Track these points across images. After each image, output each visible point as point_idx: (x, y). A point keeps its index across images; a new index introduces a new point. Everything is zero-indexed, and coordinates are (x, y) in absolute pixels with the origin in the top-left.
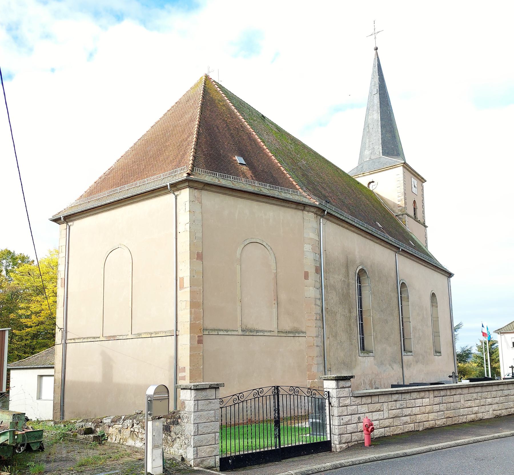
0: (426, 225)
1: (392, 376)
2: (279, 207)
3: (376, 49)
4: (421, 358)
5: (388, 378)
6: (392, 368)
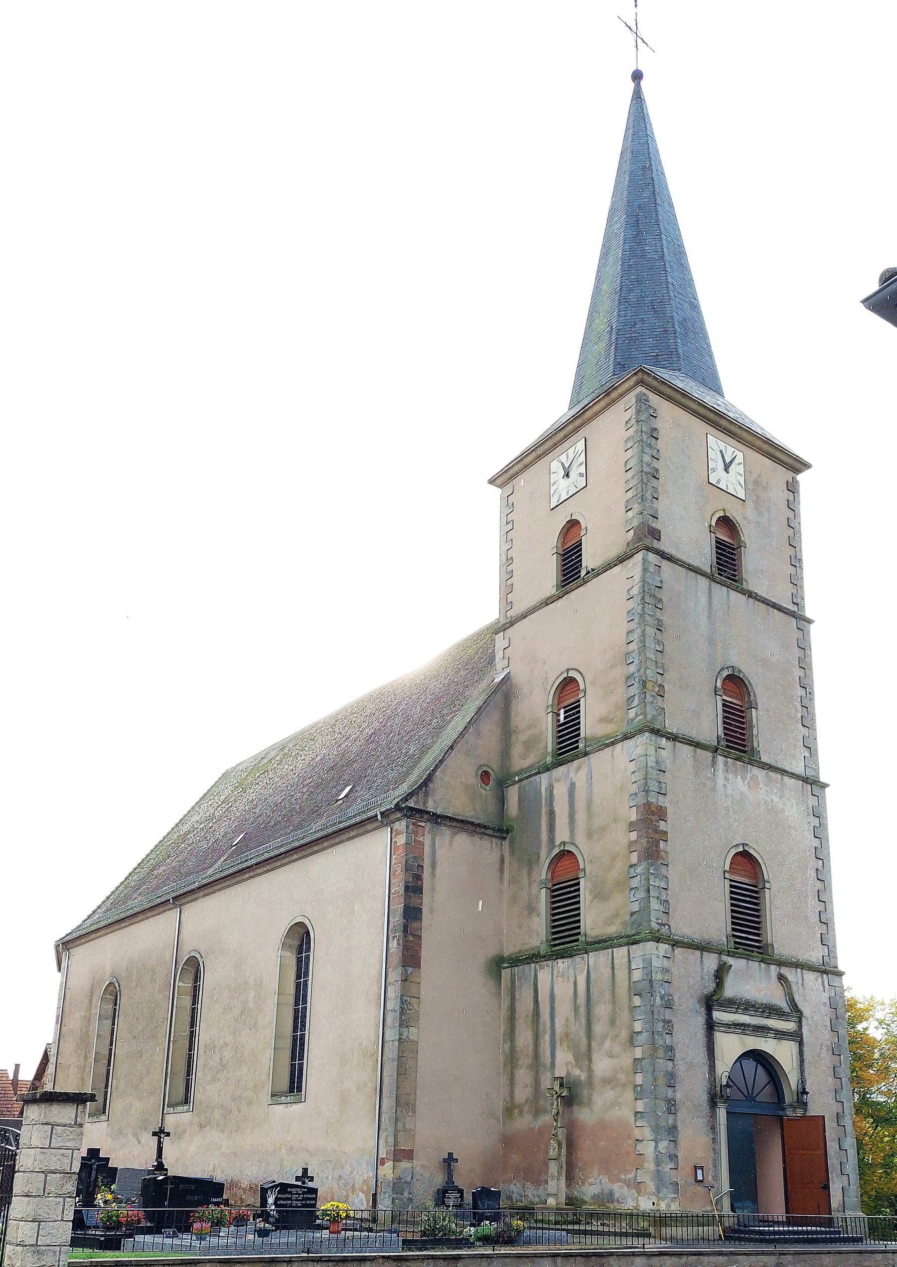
0: (822, 780)
1: (136, 1155)
2: (227, 890)
3: (637, 76)
4: (217, 1114)
5: (127, 1159)
6: (137, 1140)
